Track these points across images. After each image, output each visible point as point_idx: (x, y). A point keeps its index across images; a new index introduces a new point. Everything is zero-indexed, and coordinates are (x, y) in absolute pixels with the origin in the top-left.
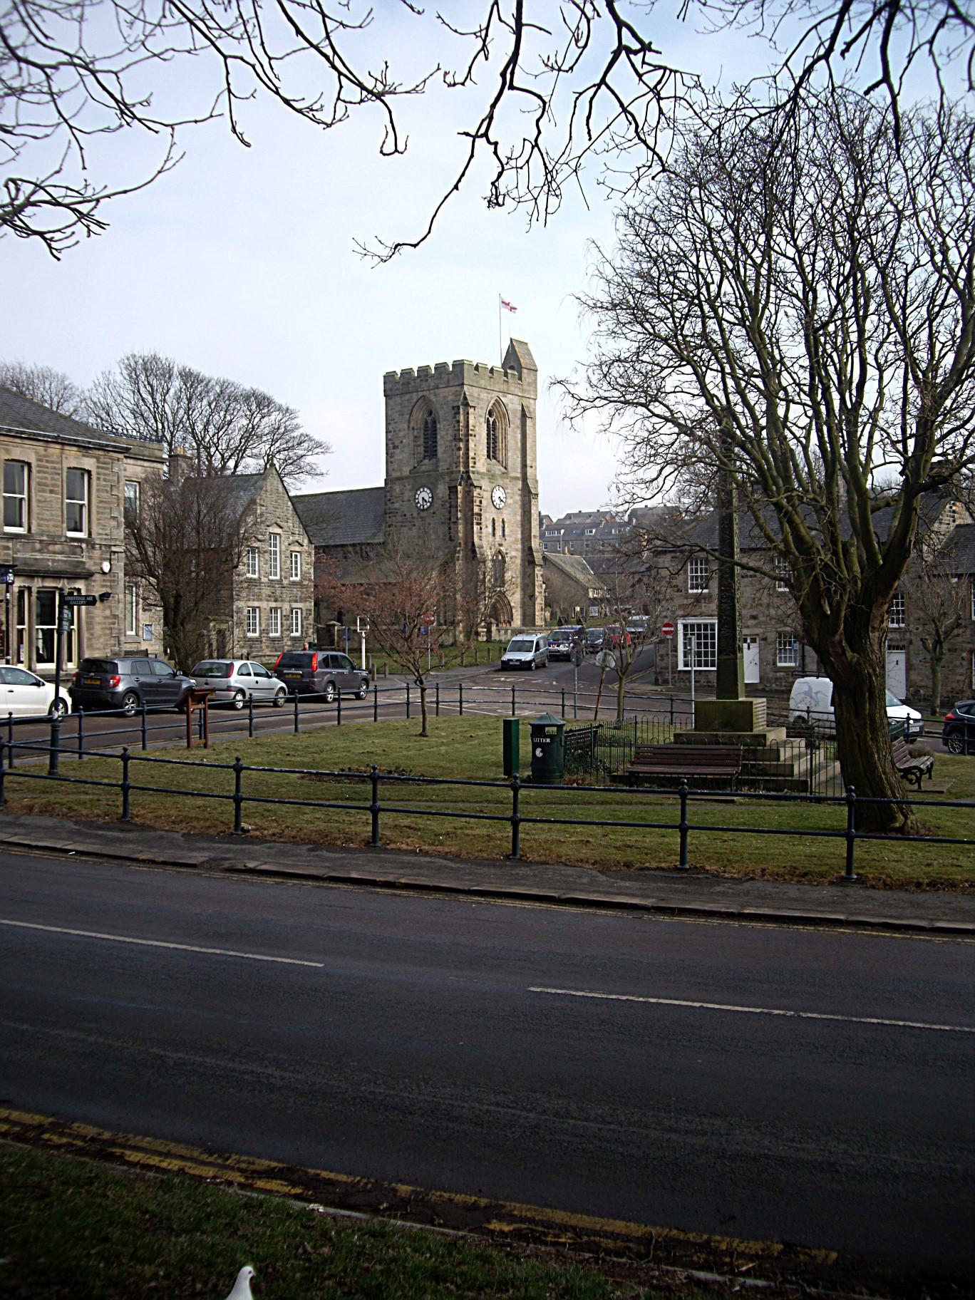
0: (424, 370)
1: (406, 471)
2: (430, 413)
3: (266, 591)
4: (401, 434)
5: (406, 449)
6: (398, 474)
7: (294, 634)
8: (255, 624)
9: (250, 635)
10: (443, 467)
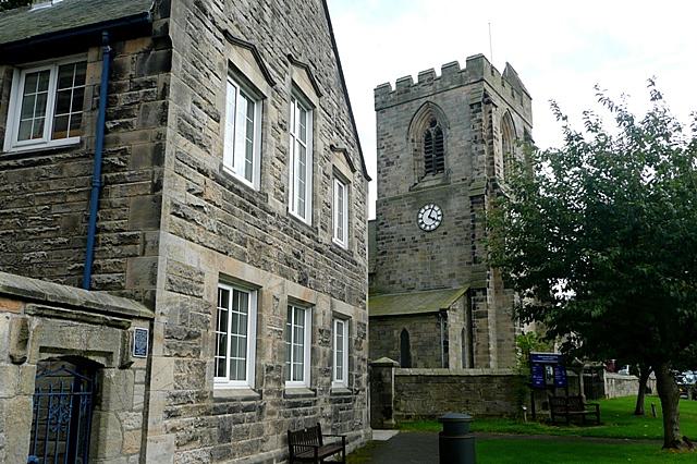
0: (427, 76)
1: (404, 188)
2: (433, 123)
3: (281, 245)
4: (398, 148)
5: (405, 165)
6: (393, 194)
7: (291, 386)
8: (238, 346)
9: (223, 385)
10: (455, 178)
